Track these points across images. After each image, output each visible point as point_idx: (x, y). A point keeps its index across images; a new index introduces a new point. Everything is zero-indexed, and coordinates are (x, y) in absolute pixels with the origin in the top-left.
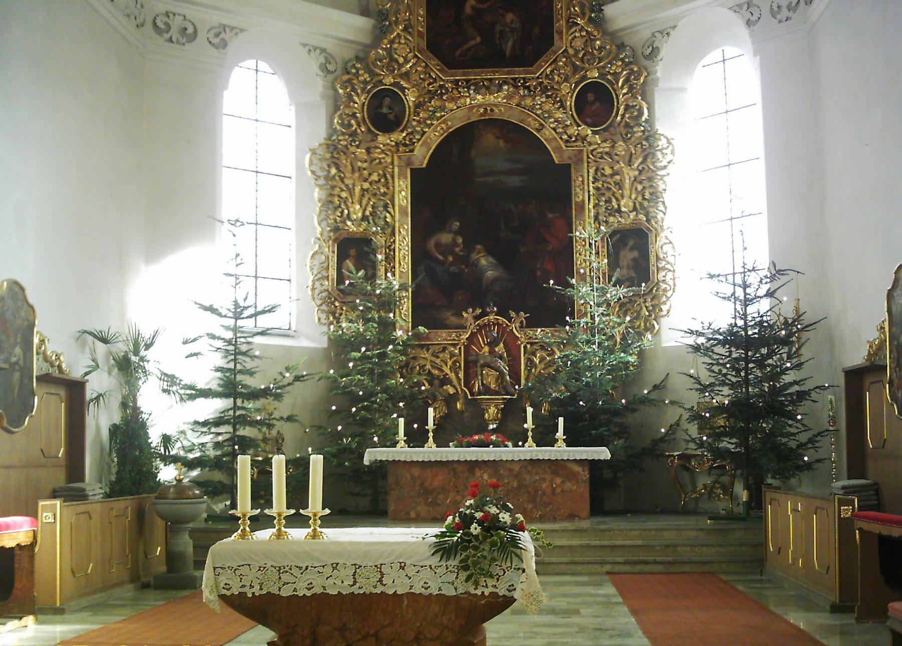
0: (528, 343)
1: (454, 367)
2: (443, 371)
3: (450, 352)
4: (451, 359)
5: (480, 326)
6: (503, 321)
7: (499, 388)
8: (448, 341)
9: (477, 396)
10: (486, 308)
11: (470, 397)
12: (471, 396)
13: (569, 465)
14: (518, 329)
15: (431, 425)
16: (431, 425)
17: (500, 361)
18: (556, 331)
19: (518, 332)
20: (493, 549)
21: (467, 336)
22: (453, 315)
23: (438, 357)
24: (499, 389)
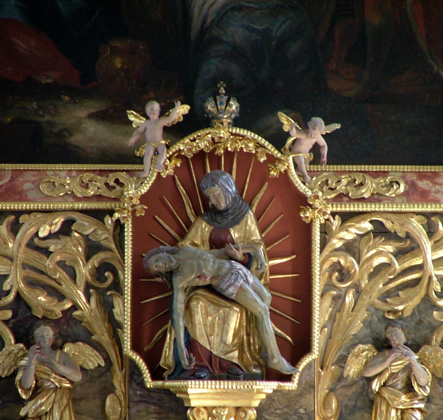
0: (333, 214)
1: (96, 284)
2: (61, 297)
3: (86, 238)
4: (88, 258)
5: (184, 158)
6: (259, 145)
7: (242, 352)
8: (78, 199)
9: (171, 377)
10: (204, 101)
11: (150, 383)
12: (154, 377)
13: (22, 302)
14: (305, 167)
15: (168, 384)
16: (168, 384)
17: (245, 270)
18: (422, 176)
19: (301, 176)
20: (163, 392)
21: (145, 189)
22: (91, 116)
23: (47, 253)
24: (241, 357)
